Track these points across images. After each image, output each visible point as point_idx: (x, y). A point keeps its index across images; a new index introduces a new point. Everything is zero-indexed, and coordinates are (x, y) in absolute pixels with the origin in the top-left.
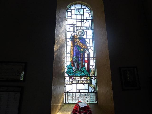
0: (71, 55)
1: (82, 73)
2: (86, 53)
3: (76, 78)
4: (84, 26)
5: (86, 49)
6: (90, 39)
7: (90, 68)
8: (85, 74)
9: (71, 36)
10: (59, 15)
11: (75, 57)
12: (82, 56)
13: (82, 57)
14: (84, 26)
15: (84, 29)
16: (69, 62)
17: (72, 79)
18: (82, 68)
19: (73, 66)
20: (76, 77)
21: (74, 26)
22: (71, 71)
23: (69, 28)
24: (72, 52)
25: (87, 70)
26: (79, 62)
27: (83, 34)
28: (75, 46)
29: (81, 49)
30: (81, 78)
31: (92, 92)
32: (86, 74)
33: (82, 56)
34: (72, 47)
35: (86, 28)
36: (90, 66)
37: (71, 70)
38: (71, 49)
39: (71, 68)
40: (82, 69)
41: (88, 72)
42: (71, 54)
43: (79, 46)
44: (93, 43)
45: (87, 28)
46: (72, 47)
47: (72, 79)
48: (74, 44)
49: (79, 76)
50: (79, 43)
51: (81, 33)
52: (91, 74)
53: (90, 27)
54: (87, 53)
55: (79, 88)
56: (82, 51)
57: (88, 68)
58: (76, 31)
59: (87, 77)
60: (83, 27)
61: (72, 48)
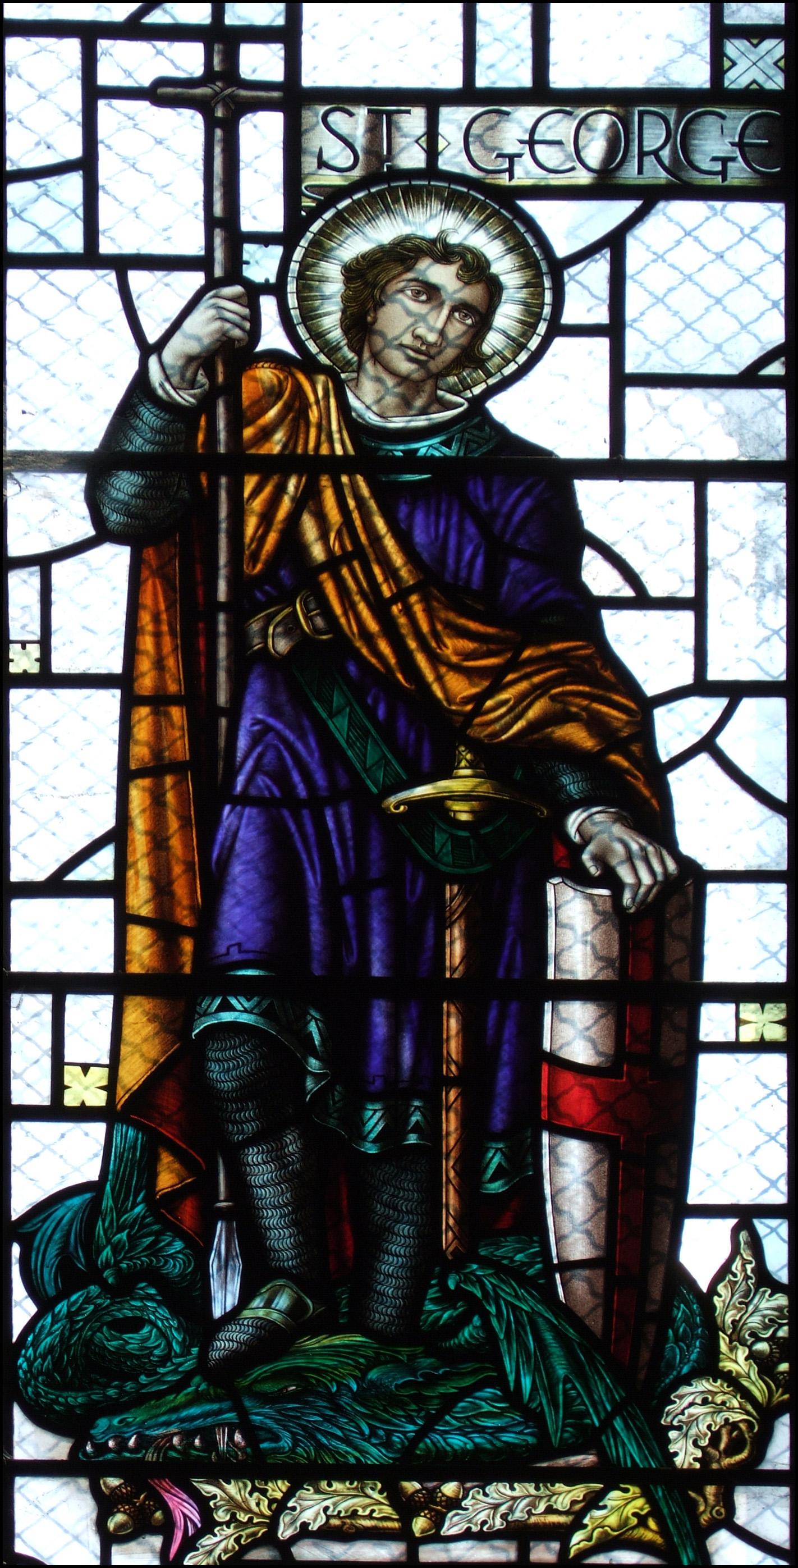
0: (139, 937)
1: (448, 1403)
2: (580, 878)
3: (280, 1506)
4: (559, 79)
5: (570, 753)
6: (715, 489)
7: (681, 1278)
8: (534, 1417)
9: (141, 384)
10: (404, 558)
11: (246, 988)
12: (456, 950)
13: (453, 990)
14: (559, 79)
15: (526, 173)
16: (83, 1114)
17: (166, 1529)
18: (459, 1262)
19: (188, 1213)
20: (277, 1489)
21: (230, 72)
22: (133, 1341)
23: (75, 151)
24: (158, 841)
25: (596, 1323)
26: (374, 1120)
27: (493, 342)
28: (257, 686)
29: (447, 773)
30: (419, 1524)
31: (563, 1495)
32: (574, 1416)
33: (456, 950)
34: (158, 702)
35: (595, 152)
36: (692, 1228)
37: (135, 1324)
38: (126, 775)
39: (154, 1276)
40: (447, 1298)
41: (622, 1375)
42: (123, 919)
43: (384, 679)
44: (217, 195)
45: (654, 136)
46: (158, 702)
47: (166, 1529)
48: (238, 637)
49: (376, 1455)
50: (380, 608)
51: (431, 292)
52: (705, 1421)
53: (737, 118)
54: (609, 879)
55: (114, 696)
56: (462, 810)
57: (611, 1284)
58: (288, 239)
59: (593, 1501)
60: (525, 115)
61: (180, 748)
